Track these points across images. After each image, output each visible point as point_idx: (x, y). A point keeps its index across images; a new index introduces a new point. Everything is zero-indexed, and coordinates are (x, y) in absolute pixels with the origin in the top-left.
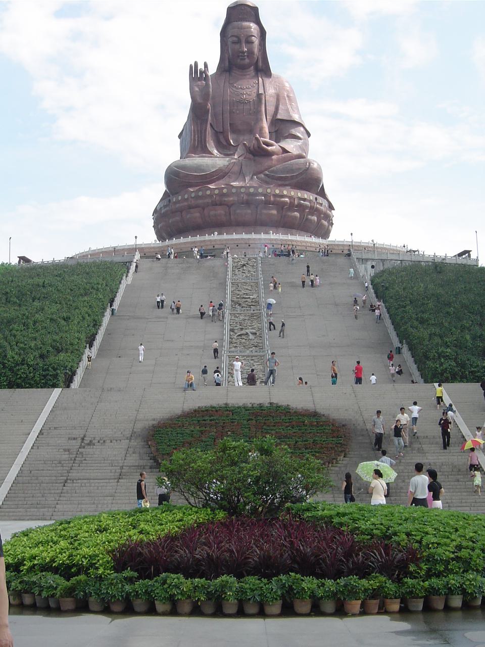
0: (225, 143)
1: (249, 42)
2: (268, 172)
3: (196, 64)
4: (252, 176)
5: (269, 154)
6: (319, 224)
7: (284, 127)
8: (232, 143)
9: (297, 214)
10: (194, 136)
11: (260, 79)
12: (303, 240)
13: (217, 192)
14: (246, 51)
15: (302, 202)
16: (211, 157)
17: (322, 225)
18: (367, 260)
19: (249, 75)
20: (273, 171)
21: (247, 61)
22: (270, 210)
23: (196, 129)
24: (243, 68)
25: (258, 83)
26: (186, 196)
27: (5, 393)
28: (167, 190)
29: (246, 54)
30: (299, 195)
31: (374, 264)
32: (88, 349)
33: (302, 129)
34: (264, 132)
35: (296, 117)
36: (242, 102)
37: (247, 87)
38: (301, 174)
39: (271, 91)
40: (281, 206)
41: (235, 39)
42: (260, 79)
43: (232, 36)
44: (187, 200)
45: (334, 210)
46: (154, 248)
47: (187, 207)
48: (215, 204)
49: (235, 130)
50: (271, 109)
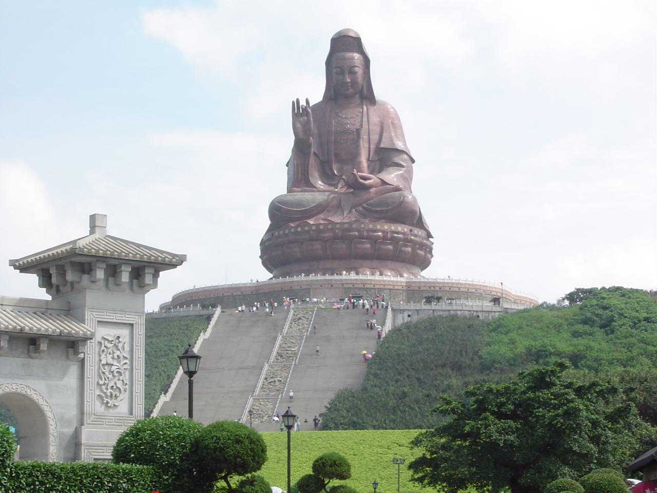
0: (330, 173)
1: (352, 73)
2: (367, 205)
3: (298, 101)
5: (367, 188)
6: (414, 253)
7: (386, 156)
8: (336, 173)
9: (390, 247)
11: (365, 107)
12: (382, 279)
13: (314, 228)
14: (349, 82)
15: (396, 235)
16: (313, 191)
17: (418, 255)
18: (404, 310)
21: (351, 90)
22: (363, 244)
24: (349, 97)
25: (363, 112)
26: (287, 231)
27: (655, 290)
29: (349, 85)
30: (393, 228)
31: (410, 313)
32: (163, 395)
33: (405, 156)
34: (362, 166)
35: (399, 145)
37: (351, 116)
39: (375, 119)
40: (374, 241)
41: (339, 70)
42: (365, 107)
44: (287, 235)
45: (432, 237)
46: (249, 287)
47: (290, 241)
48: (311, 239)
49: (340, 160)
50: (375, 138)
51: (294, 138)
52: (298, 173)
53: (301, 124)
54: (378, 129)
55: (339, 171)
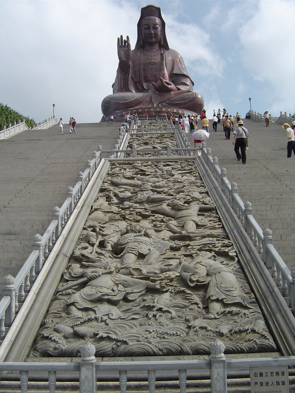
0: (140, 88)
1: (155, 28)
3: (122, 37)
4: (158, 104)
5: (170, 90)
10: (121, 81)
11: (162, 51)
19: (155, 49)
20: (171, 101)
21: (154, 40)
23: (122, 78)
24: (152, 44)
28: (104, 116)
34: (165, 76)
35: (185, 73)
36: (151, 64)
38: (190, 101)
42: (162, 51)
43: (144, 25)
49: (147, 80)
51: (119, 61)
52: (121, 84)
53: (123, 52)
54: (126, 242)
55: (146, 86)
